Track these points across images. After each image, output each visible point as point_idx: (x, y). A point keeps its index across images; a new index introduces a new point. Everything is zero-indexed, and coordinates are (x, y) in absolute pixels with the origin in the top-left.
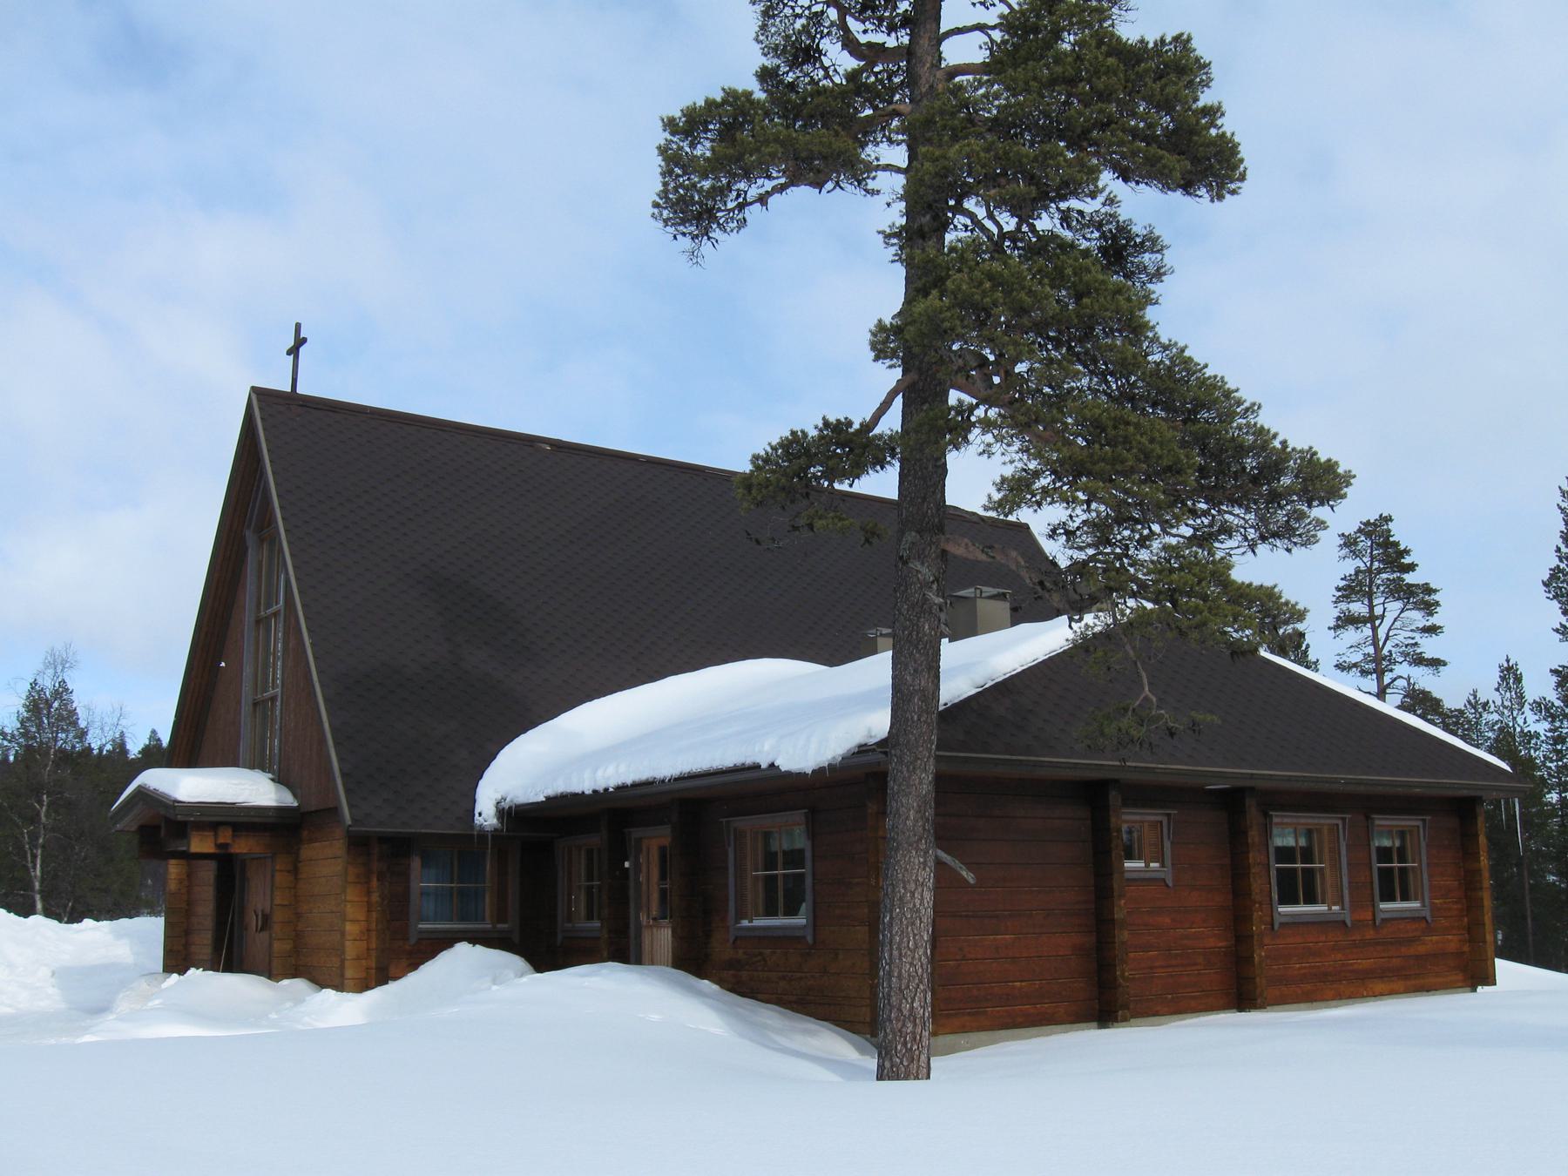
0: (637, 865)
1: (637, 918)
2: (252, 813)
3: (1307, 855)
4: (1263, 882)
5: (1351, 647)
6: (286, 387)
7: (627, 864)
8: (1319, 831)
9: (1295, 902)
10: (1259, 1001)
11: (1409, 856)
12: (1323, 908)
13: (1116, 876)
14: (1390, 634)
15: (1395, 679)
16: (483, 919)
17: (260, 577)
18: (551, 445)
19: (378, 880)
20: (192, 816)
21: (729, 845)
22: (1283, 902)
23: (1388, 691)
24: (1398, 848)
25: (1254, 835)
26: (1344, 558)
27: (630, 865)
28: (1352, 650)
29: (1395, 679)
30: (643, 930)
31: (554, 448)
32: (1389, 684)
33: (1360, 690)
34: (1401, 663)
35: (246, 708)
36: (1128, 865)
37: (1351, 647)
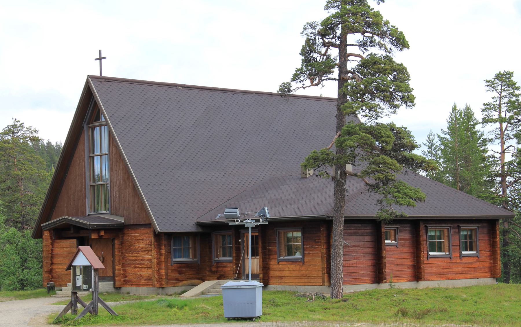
0: (243, 241)
1: (244, 255)
2: (110, 226)
3: (440, 238)
4: (424, 246)
5: (489, 132)
6: (99, 75)
7: (240, 241)
8: (443, 231)
9: (435, 251)
10: (423, 279)
11: (473, 237)
12: (443, 253)
13: (383, 245)
14: (508, 126)
15: (509, 147)
16: (189, 257)
17: (89, 141)
18: (182, 87)
19: (165, 246)
20: (94, 227)
21: (277, 236)
22: (431, 251)
23: (506, 151)
24: (469, 235)
25: (422, 232)
26: (488, 90)
27: (241, 240)
28: (490, 133)
29: (509, 147)
30: (246, 260)
31: (184, 88)
32: (506, 149)
33: (493, 151)
34: (512, 139)
35: (88, 187)
36: (386, 241)
37: (489, 132)
